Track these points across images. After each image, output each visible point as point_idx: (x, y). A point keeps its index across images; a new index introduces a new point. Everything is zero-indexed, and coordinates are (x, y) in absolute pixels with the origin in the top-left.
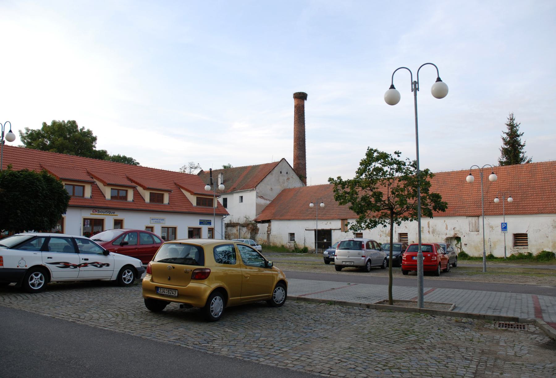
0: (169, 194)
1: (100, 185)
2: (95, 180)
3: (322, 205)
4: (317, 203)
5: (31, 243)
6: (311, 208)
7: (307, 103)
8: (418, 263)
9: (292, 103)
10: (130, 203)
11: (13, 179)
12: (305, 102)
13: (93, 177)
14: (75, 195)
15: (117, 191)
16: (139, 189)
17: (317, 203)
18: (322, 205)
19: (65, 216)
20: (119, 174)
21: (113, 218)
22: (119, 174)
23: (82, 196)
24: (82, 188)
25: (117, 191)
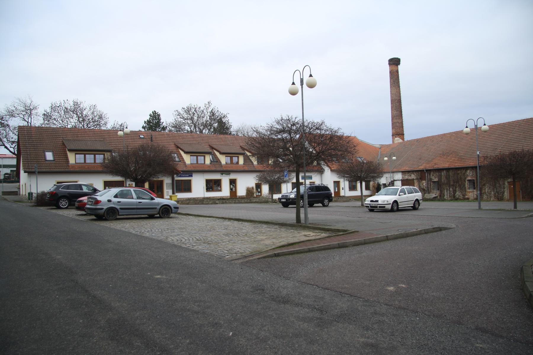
0: (243, 156)
1: (217, 154)
2: (246, 152)
3: (394, 158)
4: (390, 157)
5: (296, 188)
6: (394, 160)
7: (400, 67)
8: (475, 181)
9: (386, 69)
10: (241, 166)
11: (303, 156)
12: (399, 66)
13: (212, 148)
14: (96, 162)
15: (196, 157)
16: (217, 154)
17: (390, 157)
18: (394, 158)
19: (192, 179)
20: (237, 146)
21: (56, 181)
22: (237, 146)
23: (203, 163)
24: (237, 158)
25: (196, 157)
